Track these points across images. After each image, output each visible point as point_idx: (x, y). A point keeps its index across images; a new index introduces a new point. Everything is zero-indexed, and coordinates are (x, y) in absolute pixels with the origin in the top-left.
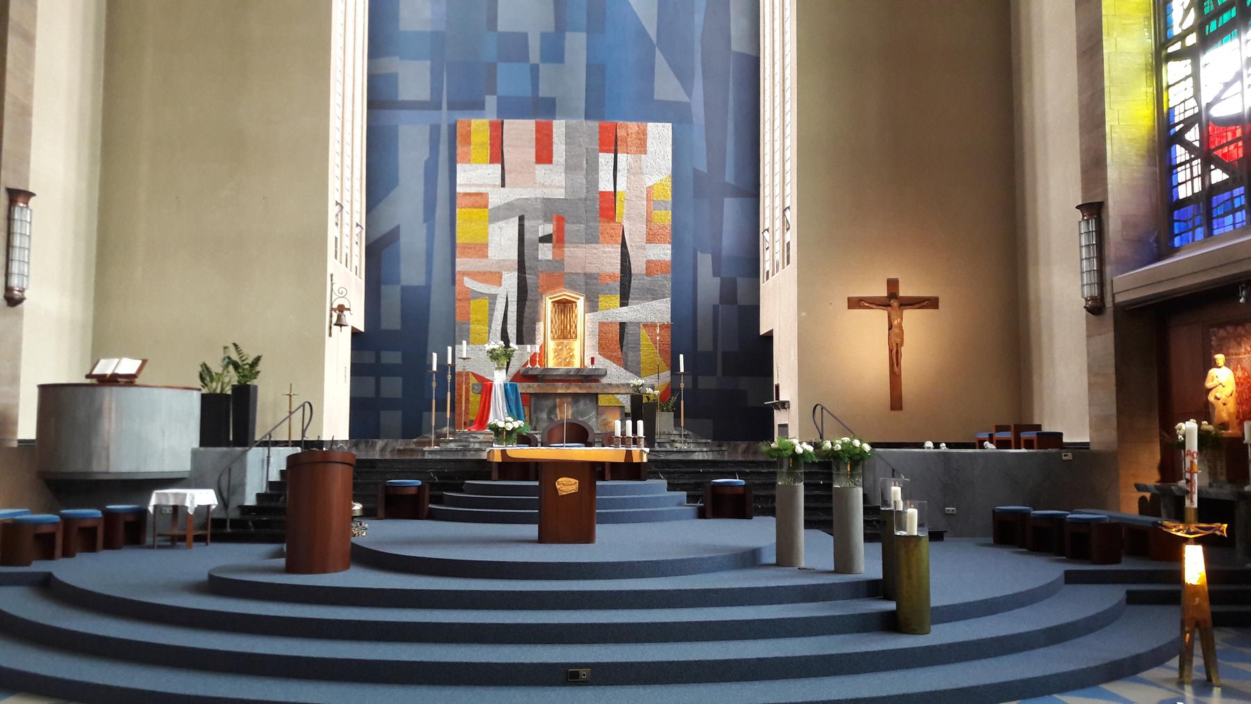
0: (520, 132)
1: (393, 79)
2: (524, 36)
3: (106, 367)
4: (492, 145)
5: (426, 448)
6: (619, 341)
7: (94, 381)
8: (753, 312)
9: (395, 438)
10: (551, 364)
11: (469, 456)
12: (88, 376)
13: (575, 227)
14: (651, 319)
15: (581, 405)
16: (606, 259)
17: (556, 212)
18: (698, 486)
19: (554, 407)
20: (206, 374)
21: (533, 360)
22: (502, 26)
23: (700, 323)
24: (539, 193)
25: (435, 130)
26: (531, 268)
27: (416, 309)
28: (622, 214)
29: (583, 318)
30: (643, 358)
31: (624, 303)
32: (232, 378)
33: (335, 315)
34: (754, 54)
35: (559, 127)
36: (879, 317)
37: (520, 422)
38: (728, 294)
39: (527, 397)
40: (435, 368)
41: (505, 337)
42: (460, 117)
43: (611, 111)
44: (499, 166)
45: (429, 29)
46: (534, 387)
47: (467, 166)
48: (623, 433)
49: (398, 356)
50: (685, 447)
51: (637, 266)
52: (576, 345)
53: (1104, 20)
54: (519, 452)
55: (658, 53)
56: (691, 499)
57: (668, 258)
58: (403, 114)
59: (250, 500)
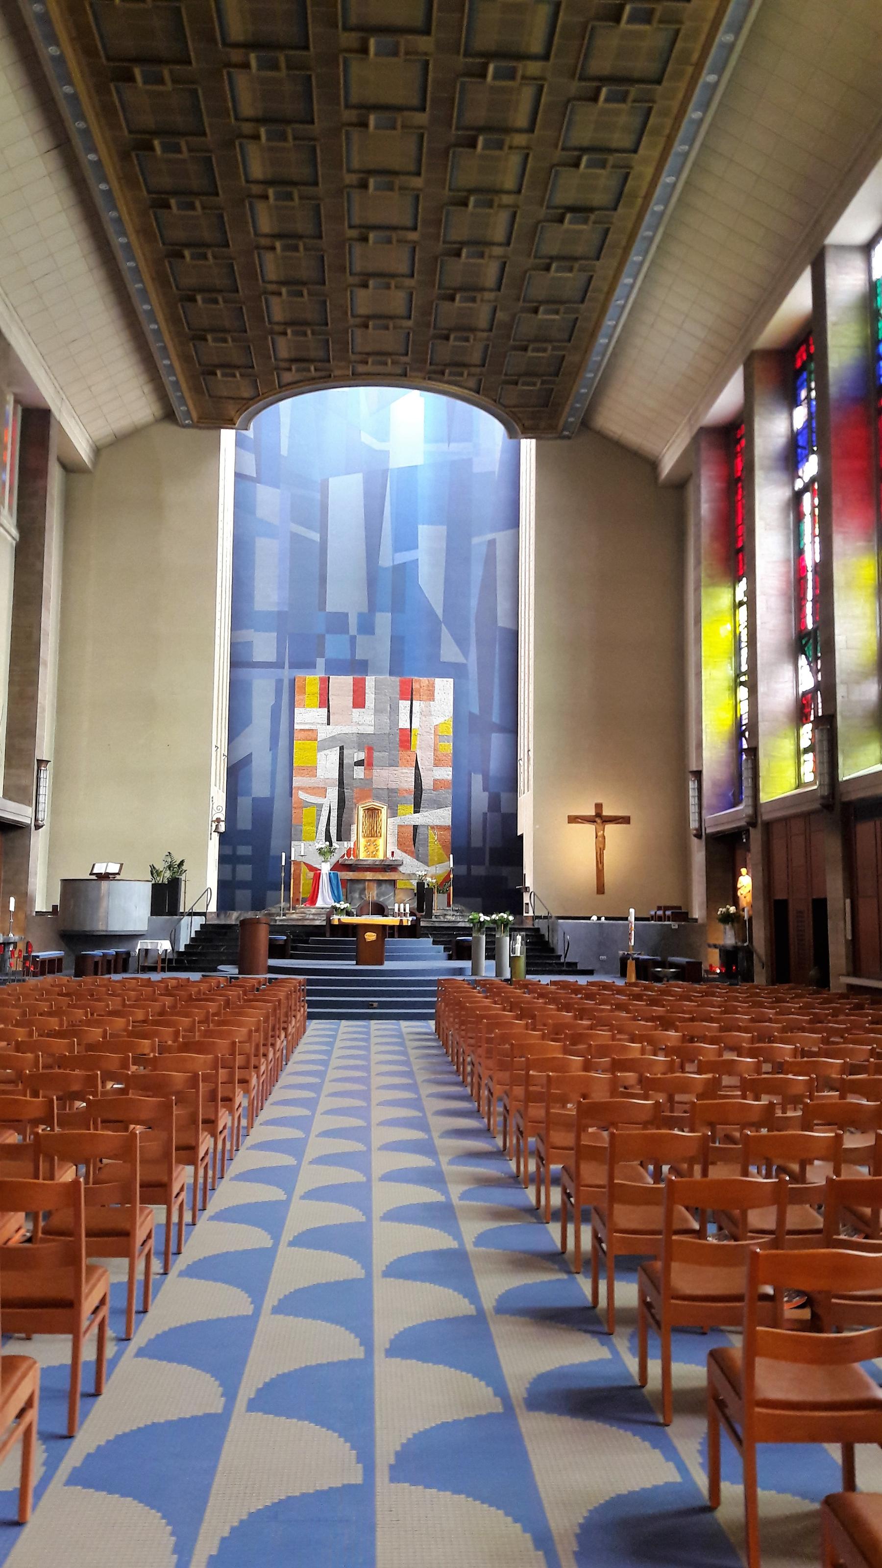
0: (342, 685)
1: (249, 644)
2: (346, 615)
3: (100, 869)
4: (321, 695)
5: (277, 918)
6: (413, 839)
7: (94, 877)
8: (512, 819)
9: (247, 910)
10: (362, 856)
11: (307, 923)
12: (91, 874)
13: (381, 754)
14: (437, 822)
15: (384, 887)
16: (405, 779)
17: (367, 743)
18: (449, 942)
19: (364, 889)
20: (154, 871)
21: (349, 853)
22: (329, 609)
23: (473, 827)
24: (354, 729)
25: (279, 682)
26: (348, 785)
27: (263, 813)
28: (415, 745)
29: (388, 825)
30: (430, 852)
31: (417, 810)
32: (168, 874)
33: (214, 825)
34: (514, 628)
35: (370, 681)
36: (589, 830)
37: (348, 905)
38: (494, 803)
39: (345, 882)
40: (283, 864)
41: (328, 838)
42: (299, 674)
43: (408, 669)
44: (326, 710)
45: (276, 609)
46: (350, 875)
47: (302, 710)
48: (399, 910)
49: (252, 848)
50: (453, 919)
51: (427, 783)
52: (381, 842)
53: (703, 659)
54: (346, 919)
55: (443, 626)
56: (445, 949)
57: (450, 777)
58: (256, 671)
59: (182, 949)
